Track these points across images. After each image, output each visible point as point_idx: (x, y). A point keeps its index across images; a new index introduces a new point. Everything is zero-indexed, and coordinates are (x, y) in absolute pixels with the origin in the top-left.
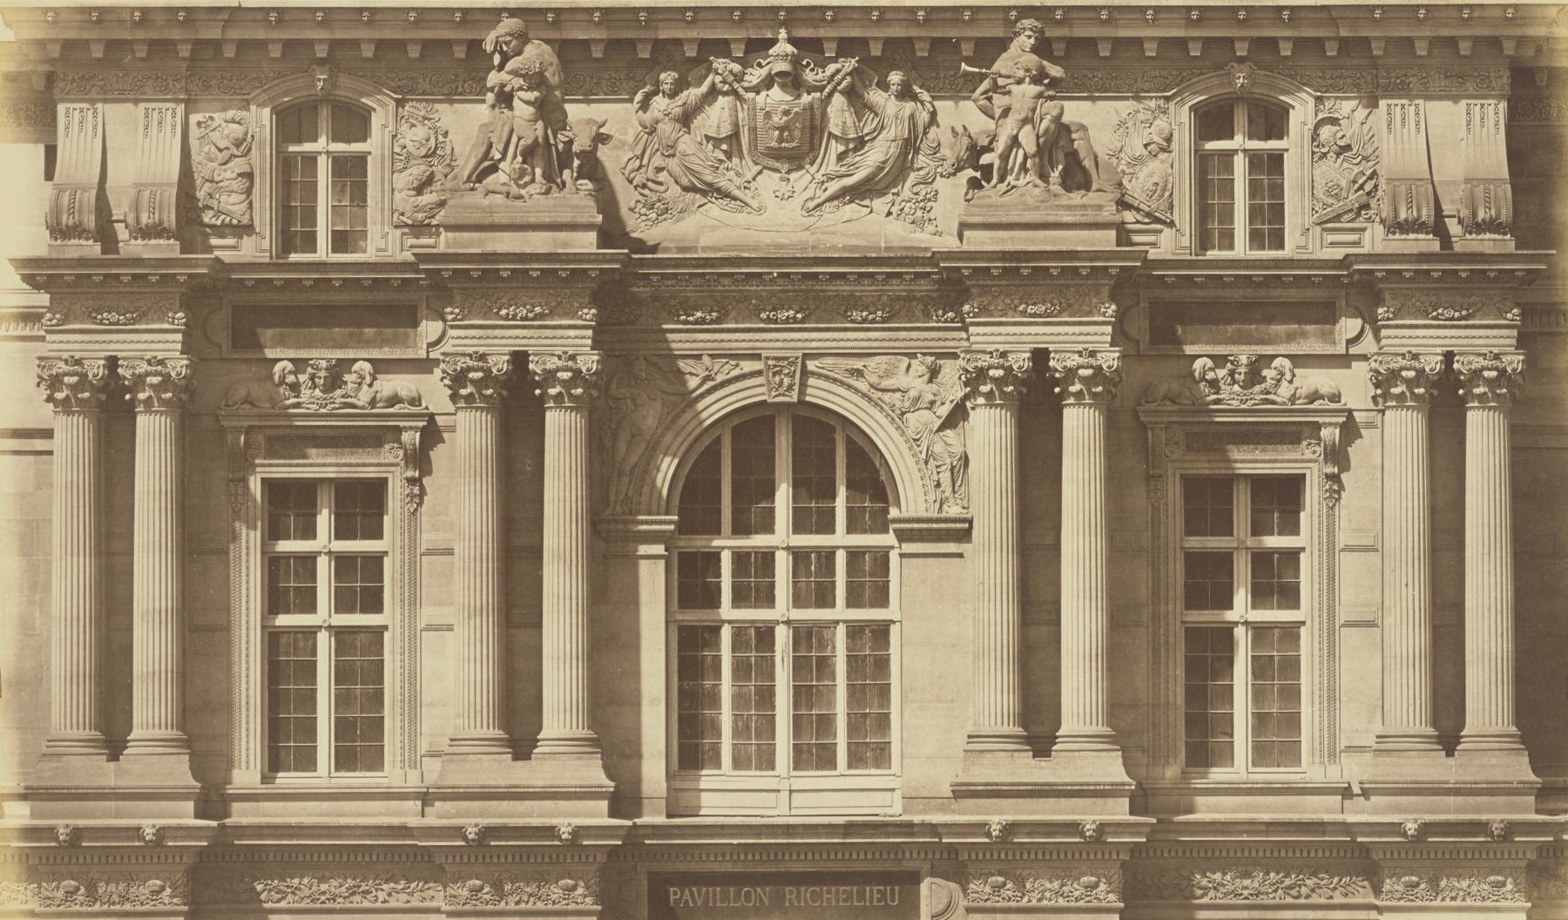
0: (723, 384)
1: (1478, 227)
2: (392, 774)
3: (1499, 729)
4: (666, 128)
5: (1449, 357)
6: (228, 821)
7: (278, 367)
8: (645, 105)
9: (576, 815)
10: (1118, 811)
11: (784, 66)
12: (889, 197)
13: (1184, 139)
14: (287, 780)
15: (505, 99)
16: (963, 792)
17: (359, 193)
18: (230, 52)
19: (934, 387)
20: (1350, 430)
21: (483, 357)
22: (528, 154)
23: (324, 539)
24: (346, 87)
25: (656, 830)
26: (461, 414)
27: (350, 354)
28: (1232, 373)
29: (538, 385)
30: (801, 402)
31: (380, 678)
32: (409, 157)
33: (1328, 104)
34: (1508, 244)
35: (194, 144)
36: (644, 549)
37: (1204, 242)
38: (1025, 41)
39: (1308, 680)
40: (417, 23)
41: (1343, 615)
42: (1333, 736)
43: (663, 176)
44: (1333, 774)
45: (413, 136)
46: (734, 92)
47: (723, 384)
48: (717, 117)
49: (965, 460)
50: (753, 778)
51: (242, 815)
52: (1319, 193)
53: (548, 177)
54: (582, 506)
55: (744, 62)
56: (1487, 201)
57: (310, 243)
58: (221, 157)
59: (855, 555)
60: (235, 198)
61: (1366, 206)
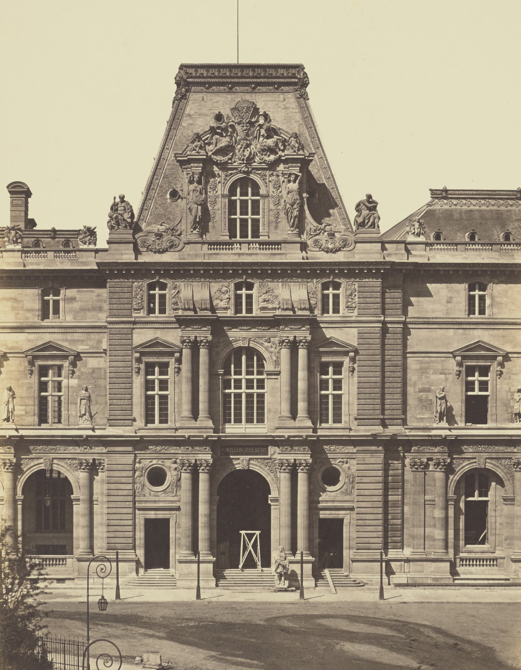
1: (202, 310)
2: (170, 424)
9: (290, 432)
34: (209, 313)
40: (472, 267)
50: (238, 425)
56: (205, 304)
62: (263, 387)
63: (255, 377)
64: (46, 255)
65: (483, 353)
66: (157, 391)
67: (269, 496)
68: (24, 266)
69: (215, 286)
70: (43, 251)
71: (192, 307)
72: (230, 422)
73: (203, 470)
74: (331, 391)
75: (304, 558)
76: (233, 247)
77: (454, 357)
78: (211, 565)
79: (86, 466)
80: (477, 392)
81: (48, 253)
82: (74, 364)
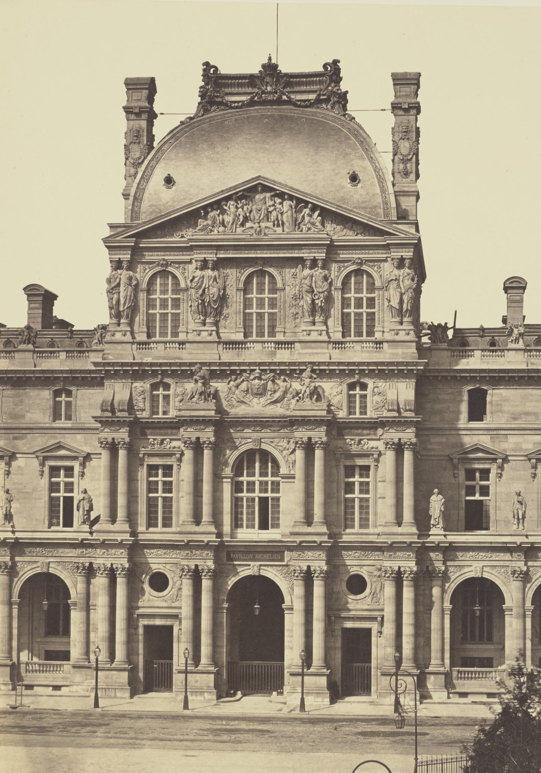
0: (243, 444)
1: (406, 411)
3: (393, 521)
4: (233, 388)
5: (400, 439)
6: (138, 538)
7: (150, 440)
8: (229, 383)
9: (209, 538)
10: (325, 538)
11: (257, 375)
12: (281, 404)
13: (345, 391)
14: (151, 529)
15: (196, 381)
16: (292, 534)
17: (168, 403)
18: (140, 372)
19: (289, 445)
20: (380, 454)
21: (190, 438)
22: (201, 394)
23: (160, 478)
24: (166, 380)
25: (227, 541)
26: (387, 452)
27: (165, 437)
28: (355, 443)
29: (403, 445)
30: (260, 449)
31: (172, 508)
32: (178, 395)
33: (376, 383)
34: (413, 415)
35: (133, 392)
36: (224, 480)
37: (350, 413)
38: (309, 369)
39: (371, 510)
41: (378, 496)
42: (376, 522)
43: (232, 399)
44: (376, 531)
45: (179, 390)
46: (247, 381)
47: (243, 444)
48: (244, 386)
49: (295, 461)
50: (250, 530)
51: (141, 537)
52: (374, 403)
53: (205, 399)
54: (211, 471)
55: (250, 374)
57: (158, 413)
58: (139, 394)
59: (273, 483)
60: (142, 404)
61: (384, 406)
62: (278, 491)
63: (270, 478)
64: (503, 354)
65: (480, 455)
66: (62, 494)
67: (69, 601)
68: (35, 366)
69: (138, 385)
70: (500, 350)
71: (395, 408)
72: (242, 526)
73: (407, 577)
74: (357, 494)
75: (188, 668)
76: (150, 346)
77: (530, 459)
78: (212, 676)
79: (82, 570)
80: (477, 497)
81: (475, 352)
82: (83, 465)
